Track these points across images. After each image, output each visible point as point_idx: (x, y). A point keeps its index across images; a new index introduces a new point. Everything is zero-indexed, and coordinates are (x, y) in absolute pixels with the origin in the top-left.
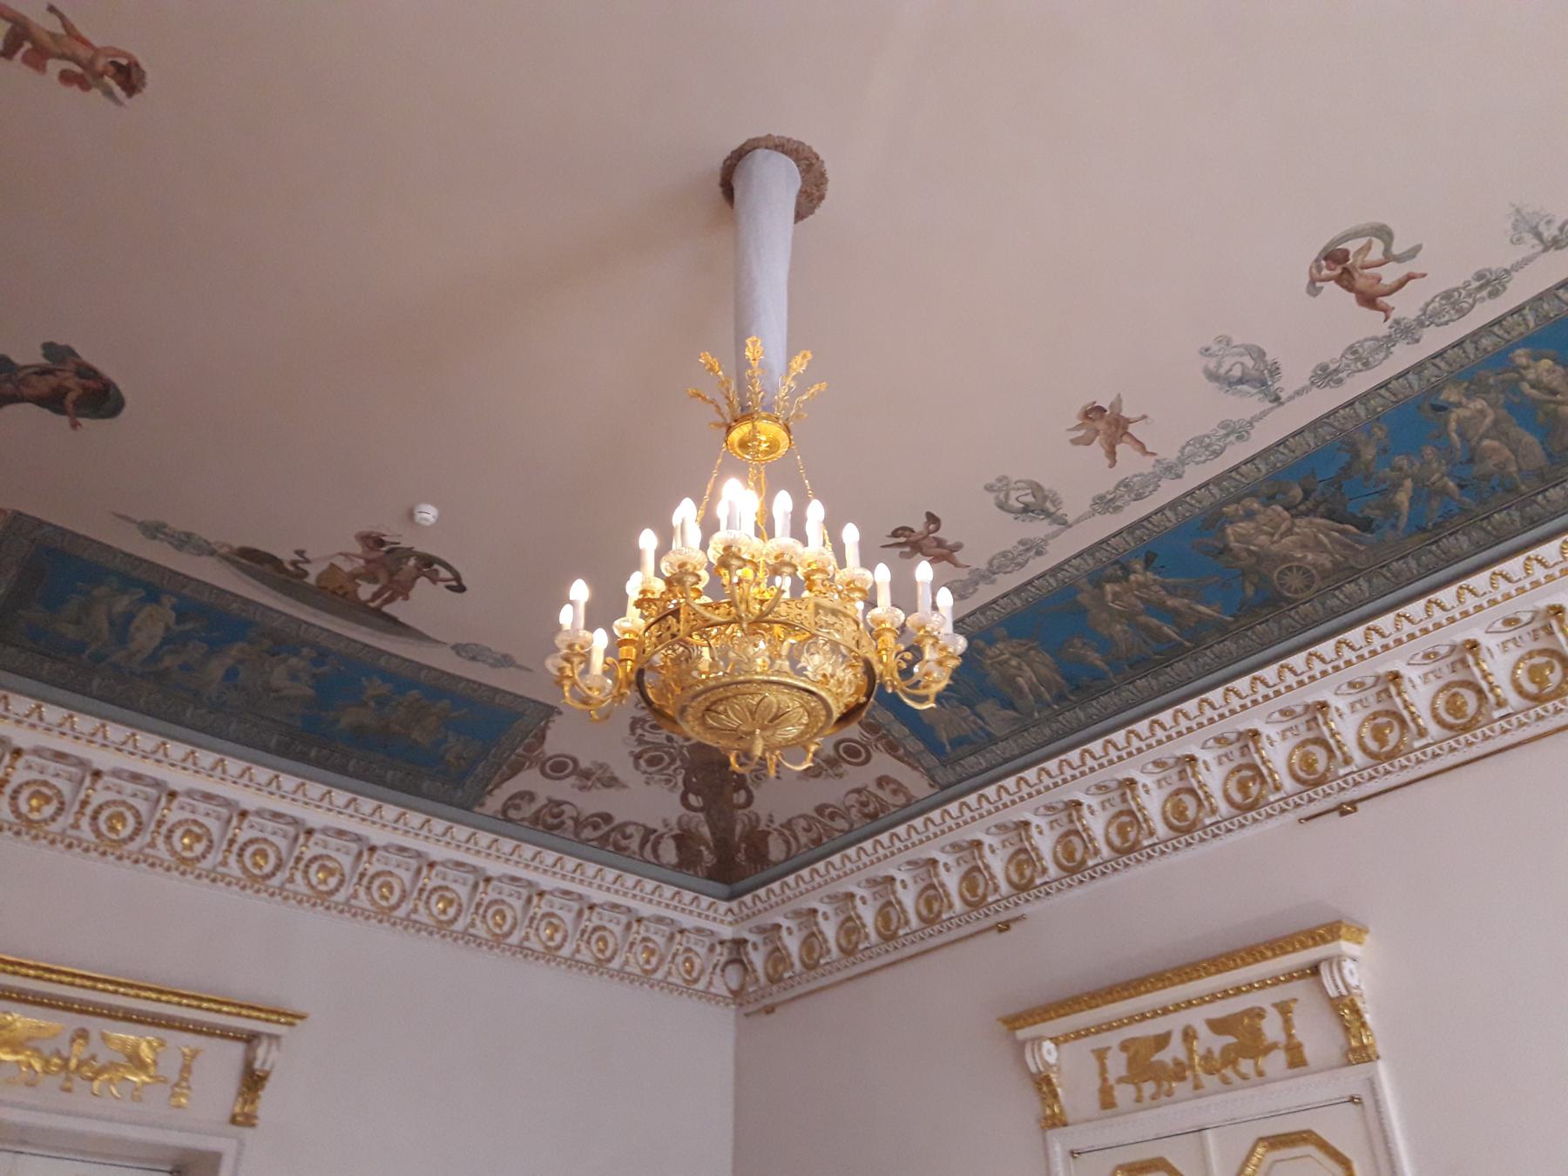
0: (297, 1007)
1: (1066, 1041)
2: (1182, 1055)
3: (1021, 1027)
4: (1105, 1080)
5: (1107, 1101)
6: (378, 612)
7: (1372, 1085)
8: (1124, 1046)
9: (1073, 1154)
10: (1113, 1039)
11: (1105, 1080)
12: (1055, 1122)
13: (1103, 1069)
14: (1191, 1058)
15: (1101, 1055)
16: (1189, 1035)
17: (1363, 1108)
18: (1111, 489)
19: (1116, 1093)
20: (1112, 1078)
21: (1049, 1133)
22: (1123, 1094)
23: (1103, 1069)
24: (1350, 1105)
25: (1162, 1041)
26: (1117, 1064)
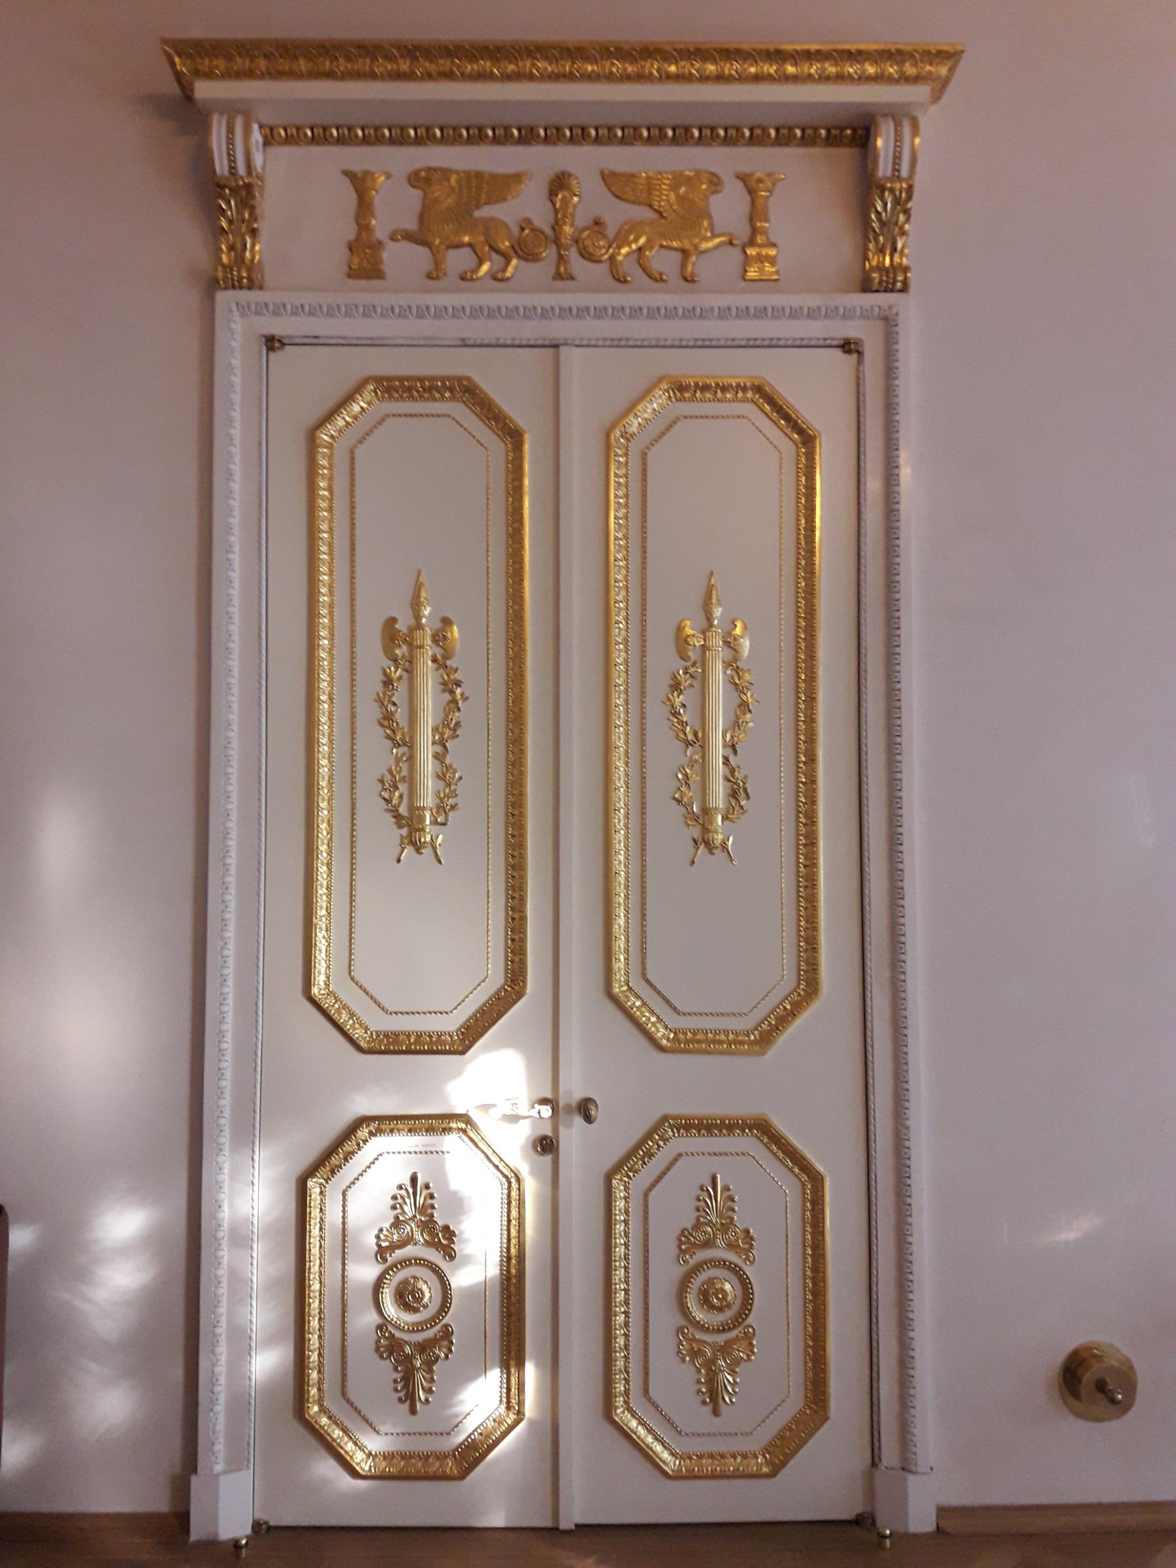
0: (940, 40)
1: (289, 141)
2: (541, 218)
3: (209, 75)
4: (363, 227)
5: (364, 260)
6: (870, 188)
7: (889, 323)
8: (420, 179)
9: (272, 343)
10: (391, 164)
11: (363, 227)
12: (239, 275)
13: (364, 208)
14: (557, 226)
15: (360, 183)
16: (559, 183)
17: (860, 360)
18: (503, 445)
19: (385, 255)
20: (380, 227)
21: (224, 298)
22: (401, 258)
23: (364, 208)
24: (838, 353)
25: (502, 186)
26: (395, 207)
